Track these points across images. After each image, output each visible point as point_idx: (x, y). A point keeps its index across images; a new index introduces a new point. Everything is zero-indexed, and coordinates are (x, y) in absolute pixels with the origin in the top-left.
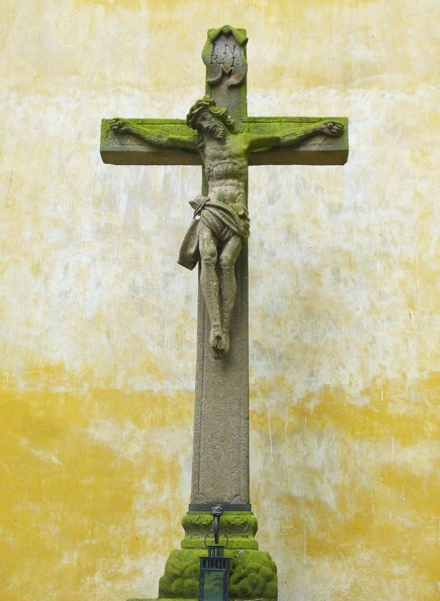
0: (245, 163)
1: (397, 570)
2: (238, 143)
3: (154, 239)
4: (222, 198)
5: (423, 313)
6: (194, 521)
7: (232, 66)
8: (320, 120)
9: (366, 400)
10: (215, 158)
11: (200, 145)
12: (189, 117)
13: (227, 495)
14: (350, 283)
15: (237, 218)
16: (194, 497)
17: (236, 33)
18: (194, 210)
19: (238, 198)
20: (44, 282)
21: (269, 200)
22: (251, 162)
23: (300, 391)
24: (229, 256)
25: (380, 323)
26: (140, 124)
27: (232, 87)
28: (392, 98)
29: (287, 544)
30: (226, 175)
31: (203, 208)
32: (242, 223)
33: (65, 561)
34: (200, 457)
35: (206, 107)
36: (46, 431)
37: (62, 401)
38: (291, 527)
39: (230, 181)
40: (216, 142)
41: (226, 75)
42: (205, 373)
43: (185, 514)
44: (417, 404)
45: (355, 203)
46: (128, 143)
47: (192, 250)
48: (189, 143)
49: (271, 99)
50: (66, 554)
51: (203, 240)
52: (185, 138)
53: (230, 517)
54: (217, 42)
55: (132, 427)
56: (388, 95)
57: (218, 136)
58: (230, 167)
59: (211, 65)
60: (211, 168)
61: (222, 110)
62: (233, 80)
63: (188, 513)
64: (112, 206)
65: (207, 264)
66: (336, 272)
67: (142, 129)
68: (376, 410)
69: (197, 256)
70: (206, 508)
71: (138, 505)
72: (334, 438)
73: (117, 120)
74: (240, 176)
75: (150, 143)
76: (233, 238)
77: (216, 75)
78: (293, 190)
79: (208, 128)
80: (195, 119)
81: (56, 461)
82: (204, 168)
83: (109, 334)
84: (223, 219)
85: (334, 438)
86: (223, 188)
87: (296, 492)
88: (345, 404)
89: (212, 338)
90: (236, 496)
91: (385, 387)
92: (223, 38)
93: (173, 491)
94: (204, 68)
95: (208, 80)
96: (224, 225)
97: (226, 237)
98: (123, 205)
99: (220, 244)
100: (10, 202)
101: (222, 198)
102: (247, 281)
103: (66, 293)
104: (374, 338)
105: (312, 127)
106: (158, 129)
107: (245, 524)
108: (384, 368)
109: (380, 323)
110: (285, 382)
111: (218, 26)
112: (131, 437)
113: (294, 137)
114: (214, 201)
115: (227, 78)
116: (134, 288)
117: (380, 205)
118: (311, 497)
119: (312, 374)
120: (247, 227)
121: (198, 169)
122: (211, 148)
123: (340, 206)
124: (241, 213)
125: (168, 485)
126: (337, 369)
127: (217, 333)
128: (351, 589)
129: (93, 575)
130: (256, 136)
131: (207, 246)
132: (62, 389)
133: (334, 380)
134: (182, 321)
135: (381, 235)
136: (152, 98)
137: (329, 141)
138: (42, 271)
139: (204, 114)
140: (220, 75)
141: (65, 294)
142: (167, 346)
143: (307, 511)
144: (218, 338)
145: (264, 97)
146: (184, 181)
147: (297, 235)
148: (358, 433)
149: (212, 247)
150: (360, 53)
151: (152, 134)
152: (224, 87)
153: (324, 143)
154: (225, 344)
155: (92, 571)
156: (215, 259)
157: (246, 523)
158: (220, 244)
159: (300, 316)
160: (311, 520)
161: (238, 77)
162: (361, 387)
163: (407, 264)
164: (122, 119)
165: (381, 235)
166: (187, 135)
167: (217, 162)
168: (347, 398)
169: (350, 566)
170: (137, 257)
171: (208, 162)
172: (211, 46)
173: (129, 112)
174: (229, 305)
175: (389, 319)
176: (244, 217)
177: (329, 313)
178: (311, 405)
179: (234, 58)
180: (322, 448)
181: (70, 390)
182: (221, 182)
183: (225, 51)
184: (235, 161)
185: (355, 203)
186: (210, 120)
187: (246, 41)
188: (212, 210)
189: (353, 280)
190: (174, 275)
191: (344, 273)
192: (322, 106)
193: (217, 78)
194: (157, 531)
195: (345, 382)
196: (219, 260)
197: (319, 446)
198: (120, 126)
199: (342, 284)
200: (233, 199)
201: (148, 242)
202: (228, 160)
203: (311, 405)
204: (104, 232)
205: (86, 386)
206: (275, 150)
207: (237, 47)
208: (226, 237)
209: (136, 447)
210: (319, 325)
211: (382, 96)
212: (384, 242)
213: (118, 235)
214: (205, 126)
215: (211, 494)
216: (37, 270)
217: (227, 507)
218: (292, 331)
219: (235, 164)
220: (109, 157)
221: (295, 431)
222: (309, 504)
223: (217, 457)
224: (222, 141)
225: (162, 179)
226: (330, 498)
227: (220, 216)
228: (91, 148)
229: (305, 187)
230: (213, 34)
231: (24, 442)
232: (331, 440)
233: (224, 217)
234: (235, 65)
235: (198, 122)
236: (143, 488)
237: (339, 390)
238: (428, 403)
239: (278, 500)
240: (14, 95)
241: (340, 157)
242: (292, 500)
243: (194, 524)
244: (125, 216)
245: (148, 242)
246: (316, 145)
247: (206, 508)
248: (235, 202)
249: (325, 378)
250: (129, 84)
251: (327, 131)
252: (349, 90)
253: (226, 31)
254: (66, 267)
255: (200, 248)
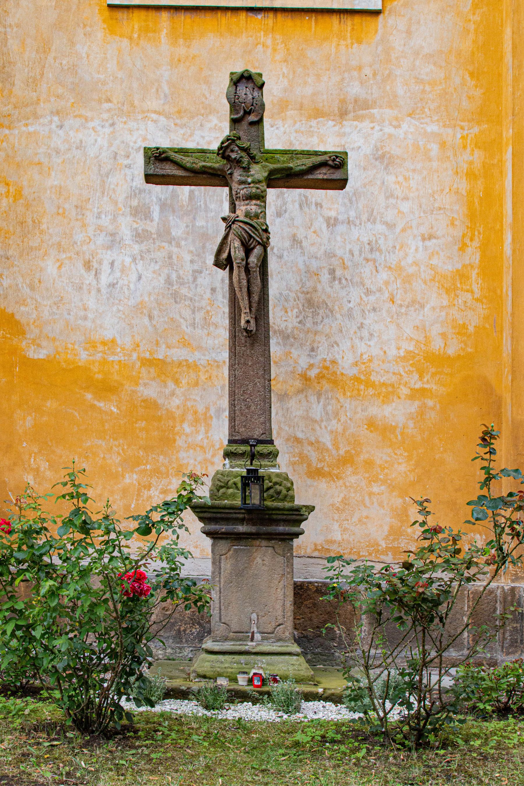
0: (266, 187)
1: (375, 489)
2: (258, 172)
3: (183, 243)
4: (247, 215)
5: (401, 306)
6: (233, 450)
7: (252, 105)
8: (325, 153)
9: (354, 371)
10: (241, 183)
11: (229, 172)
12: (220, 149)
13: (257, 433)
14: (344, 281)
15: (260, 231)
16: (230, 435)
17: (255, 77)
18: (225, 224)
19: (261, 215)
20: (96, 275)
21: (277, 213)
22: (269, 186)
23: (303, 362)
24: (255, 261)
25: (367, 313)
26: (176, 152)
27: (252, 124)
28: (381, 130)
29: (294, 471)
30: (250, 197)
31: (233, 223)
32: (265, 235)
33: (127, 481)
34: (235, 407)
35: (233, 141)
36: (107, 388)
37: (117, 367)
38: (297, 459)
39: (254, 202)
40: (241, 170)
41: (247, 113)
42: (237, 348)
43: (225, 446)
44: (394, 373)
45: (348, 218)
46: (165, 167)
47: (225, 255)
48: (219, 170)
49: (277, 128)
50: (127, 476)
51: (235, 248)
52: (216, 166)
53: (259, 448)
54: (238, 84)
55: (173, 386)
56: (377, 128)
57: (244, 165)
58: (254, 191)
59: (234, 106)
60: (238, 191)
61: (246, 145)
62: (252, 118)
63: (227, 446)
64: (148, 216)
65: (239, 267)
66: (332, 272)
67: (178, 157)
68: (362, 377)
69: (229, 260)
70: (244, 442)
71: (180, 442)
72: (330, 397)
73: (158, 149)
74: (261, 197)
75: (185, 169)
76: (258, 247)
77: (237, 114)
78: (297, 206)
79: (235, 159)
80: (223, 151)
81: (115, 410)
82: (231, 190)
83: (150, 317)
84: (250, 232)
85: (330, 397)
86: (249, 207)
87: (300, 435)
88: (338, 373)
89: (243, 322)
90: (262, 434)
91: (370, 361)
92: (244, 80)
93: (207, 432)
94: (228, 106)
95: (232, 117)
96: (250, 237)
97: (252, 246)
98: (156, 214)
99: (248, 251)
100: (61, 211)
101: (247, 215)
102: (268, 279)
103: (114, 284)
104: (362, 324)
105: (319, 159)
106: (192, 156)
107: (270, 453)
108: (370, 346)
109: (367, 313)
110: (292, 355)
111: (239, 69)
112: (173, 394)
113: (304, 167)
114: (242, 218)
115: (247, 116)
116: (168, 281)
117: (369, 220)
118: (313, 439)
119: (313, 350)
120: (268, 238)
121: (226, 190)
122: (237, 175)
123: (336, 219)
124: (264, 228)
125: (203, 428)
126: (333, 346)
127: (247, 318)
128: (342, 501)
129: (149, 490)
130: (272, 166)
131: (238, 253)
132: (116, 358)
133: (330, 355)
134: (209, 308)
135: (369, 244)
136: (176, 125)
137: (332, 171)
138: (93, 266)
139: (232, 147)
140: (242, 113)
141: (113, 285)
142: (198, 327)
143: (310, 448)
144: (248, 322)
145: (272, 126)
146: (215, 201)
147: (301, 242)
148: (349, 394)
149: (241, 254)
150: (355, 89)
151: (187, 161)
152: (244, 124)
153: (326, 171)
154: (252, 326)
155: (149, 487)
156: (244, 262)
157: (271, 452)
158: (248, 251)
159: (303, 306)
160: (313, 456)
161: (257, 116)
162: (350, 362)
163: (390, 268)
164: (162, 148)
165: (369, 244)
166: (217, 163)
167: (243, 186)
168: (340, 368)
169: (341, 486)
170: (170, 257)
171: (235, 186)
172: (234, 87)
173: (164, 142)
174: (256, 297)
175: (374, 310)
176: (266, 231)
177: (326, 304)
178: (313, 373)
179: (253, 98)
180: (321, 403)
181: (122, 358)
182: (247, 202)
183: (245, 91)
184: (257, 185)
185: (348, 218)
186: (237, 152)
187: (263, 84)
188: (241, 224)
189: (346, 279)
190: (201, 272)
191: (338, 273)
192: (324, 139)
193: (239, 115)
194: (195, 460)
195: (338, 357)
196: (247, 264)
197: (319, 402)
198: (160, 154)
199: (337, 282)
200: (257, 216)
201: (178, 246)
202: (252, 185)
203: (313, 373)
204: (140, 236)
205: (135, 356)
206: (287, 176)
207: (256, 89)
208: (252, 246)
209: (176, 402)
210: (319, 313)
211: (373, 128)
212: (372, 250)
213: (154, 239)
214: (233, 157)
215: (244, 433)
216: (88, 265)
217: (260, 442)
218: (297, 317)
219: (258, 188)
220: (149, 178)
221: (300, 391)
222: (311, 444)
223: (249, 407)
224: (246, 169)
225: (188, 194)
226: (327, 440)
227: (248, 230)
228: (126, 166)
229: (307, 204)
230: (235, 78)
231: (89, 396)
232: (328, 398)
233: (251, 230)
234: (255, 105)
235: (227, 154)
236: (184, 430)
237: (334, 362)
238: (403, 374)
239: (288, 440)
240: (56, 119)
241: (340, 184)
242: (297, 440)
243: (232, 453)
244: (158, 224)
245: (178, 246)
246: (321, 175)
247: (244, 442)
248: (258, 219)
249: (323, 353)
250: (155, 112)
251: (330, 163)
252: (344, 122)
253: (246, 75)
254: (112, 264)
255: (232, 254)
